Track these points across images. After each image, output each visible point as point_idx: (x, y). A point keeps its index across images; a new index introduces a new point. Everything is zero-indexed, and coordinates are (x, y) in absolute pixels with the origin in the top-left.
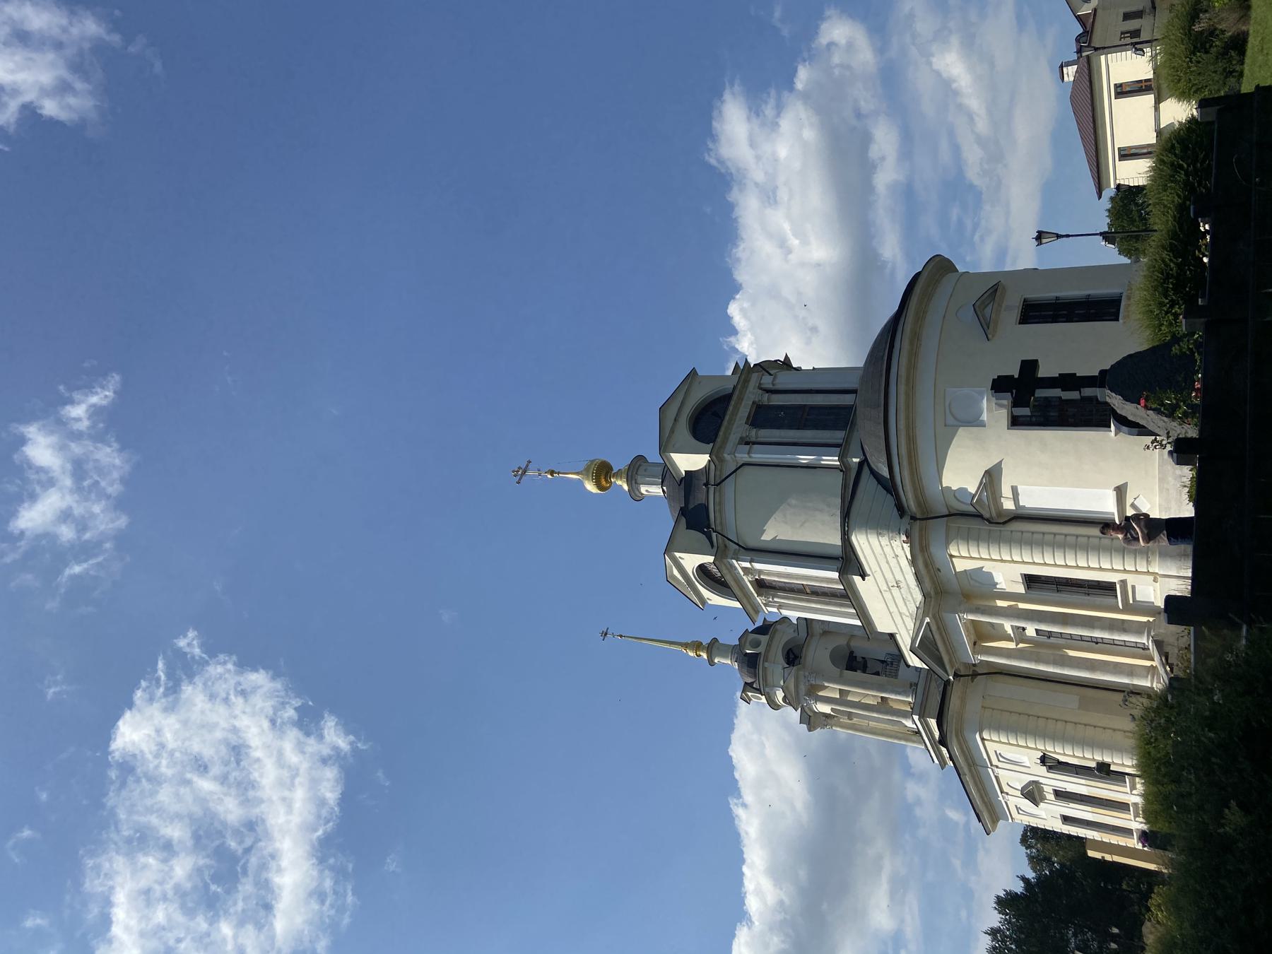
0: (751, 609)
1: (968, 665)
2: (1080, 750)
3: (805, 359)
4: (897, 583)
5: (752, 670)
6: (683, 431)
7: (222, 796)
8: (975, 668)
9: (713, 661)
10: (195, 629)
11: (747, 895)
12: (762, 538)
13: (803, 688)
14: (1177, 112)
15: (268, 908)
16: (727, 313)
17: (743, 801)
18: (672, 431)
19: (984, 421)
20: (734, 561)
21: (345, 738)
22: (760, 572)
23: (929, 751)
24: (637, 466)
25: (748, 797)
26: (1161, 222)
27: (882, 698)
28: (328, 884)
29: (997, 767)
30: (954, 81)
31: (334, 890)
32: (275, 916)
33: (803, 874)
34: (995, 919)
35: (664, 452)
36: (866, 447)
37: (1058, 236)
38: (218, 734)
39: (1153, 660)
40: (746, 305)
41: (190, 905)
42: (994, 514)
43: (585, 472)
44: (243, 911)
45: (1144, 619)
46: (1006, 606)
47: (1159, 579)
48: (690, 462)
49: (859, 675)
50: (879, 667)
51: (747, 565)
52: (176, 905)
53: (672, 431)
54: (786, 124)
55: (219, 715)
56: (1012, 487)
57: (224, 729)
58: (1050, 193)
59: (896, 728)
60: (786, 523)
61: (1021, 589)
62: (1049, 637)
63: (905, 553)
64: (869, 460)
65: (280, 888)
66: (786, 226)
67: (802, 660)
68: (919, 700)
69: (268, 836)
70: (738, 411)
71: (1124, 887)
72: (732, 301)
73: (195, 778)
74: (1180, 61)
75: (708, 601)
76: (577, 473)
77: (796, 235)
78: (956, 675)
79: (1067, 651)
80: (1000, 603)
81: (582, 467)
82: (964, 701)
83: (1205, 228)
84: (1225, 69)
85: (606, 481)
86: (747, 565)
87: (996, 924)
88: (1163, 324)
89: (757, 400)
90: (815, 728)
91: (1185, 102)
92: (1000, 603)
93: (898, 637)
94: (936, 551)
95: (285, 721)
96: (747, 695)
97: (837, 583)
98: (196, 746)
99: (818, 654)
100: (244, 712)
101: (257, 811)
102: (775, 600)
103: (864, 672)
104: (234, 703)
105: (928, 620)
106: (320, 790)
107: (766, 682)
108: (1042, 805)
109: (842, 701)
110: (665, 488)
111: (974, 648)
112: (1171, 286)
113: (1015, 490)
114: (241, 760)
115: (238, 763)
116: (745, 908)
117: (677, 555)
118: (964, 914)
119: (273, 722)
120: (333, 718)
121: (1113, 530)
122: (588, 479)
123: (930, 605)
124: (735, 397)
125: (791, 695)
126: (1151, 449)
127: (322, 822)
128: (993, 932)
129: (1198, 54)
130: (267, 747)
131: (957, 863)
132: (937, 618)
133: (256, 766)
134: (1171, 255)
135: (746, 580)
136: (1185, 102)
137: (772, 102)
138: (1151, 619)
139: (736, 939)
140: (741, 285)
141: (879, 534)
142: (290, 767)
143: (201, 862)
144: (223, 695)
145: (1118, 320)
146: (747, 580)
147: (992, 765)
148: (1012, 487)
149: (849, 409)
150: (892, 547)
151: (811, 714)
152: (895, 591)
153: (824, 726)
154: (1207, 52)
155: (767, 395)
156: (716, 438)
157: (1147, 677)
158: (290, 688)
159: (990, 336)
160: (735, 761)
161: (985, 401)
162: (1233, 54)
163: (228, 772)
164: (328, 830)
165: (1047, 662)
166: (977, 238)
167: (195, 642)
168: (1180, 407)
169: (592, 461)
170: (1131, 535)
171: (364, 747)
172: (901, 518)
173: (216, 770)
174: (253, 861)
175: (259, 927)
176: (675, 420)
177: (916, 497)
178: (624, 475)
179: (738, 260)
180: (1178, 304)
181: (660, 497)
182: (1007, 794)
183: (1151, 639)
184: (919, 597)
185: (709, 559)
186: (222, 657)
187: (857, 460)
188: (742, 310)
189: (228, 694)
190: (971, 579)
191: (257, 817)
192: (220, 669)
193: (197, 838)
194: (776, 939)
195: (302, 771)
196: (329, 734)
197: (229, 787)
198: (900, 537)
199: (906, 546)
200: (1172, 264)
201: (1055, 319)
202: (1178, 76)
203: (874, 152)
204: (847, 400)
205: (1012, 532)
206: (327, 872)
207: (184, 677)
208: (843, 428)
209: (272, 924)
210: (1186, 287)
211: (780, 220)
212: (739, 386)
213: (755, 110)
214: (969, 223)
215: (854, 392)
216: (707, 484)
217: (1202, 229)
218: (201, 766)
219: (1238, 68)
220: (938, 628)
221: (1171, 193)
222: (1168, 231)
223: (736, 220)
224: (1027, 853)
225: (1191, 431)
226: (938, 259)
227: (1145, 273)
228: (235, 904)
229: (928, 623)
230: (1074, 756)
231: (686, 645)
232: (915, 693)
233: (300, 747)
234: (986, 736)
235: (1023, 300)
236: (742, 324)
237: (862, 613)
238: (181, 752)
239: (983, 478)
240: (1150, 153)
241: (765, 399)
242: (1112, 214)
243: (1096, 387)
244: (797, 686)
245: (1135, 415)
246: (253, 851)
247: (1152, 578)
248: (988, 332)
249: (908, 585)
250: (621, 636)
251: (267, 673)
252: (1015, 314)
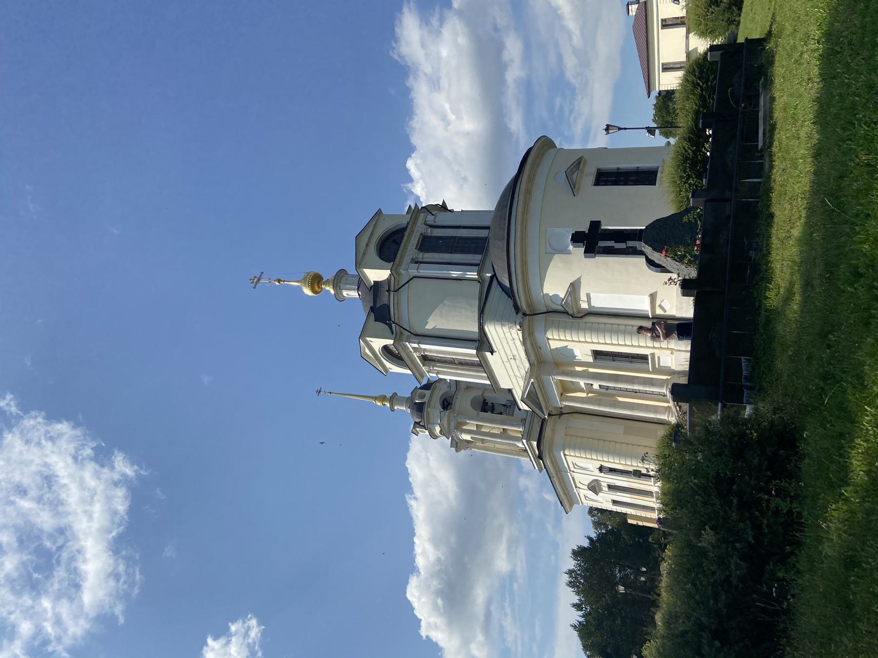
0: (418, 374)
1: (556, 408)
2: (624, 459)
3: (456, 205)
4: (513, 356)
5: (420, 413)
6: (372, 251)
7: (39, 511)
8: (561, 410)
9: (393, 409)
10: (11, 393)
11: (417, 556)
12: (426, 328)
13: (453, 424)
14: (700, 45)
15: (77, 587)
16: (406, 167)
17: (414, 496)
18: (364, 254)
19: (570, 250)
20: (407, 343)
21: (131, 468)
22: (425, 350)
23: (532, 462)
24: (340, 277)
25: (418, 493)
26: (684, 121)
27: (503, 429)
28: (121, 568)
29: (573, 472)
30: (560, 9)
31: (126, 572)
32: (83, 592)
33: (453, 539)
34: (571, 564)
35: (359, 268)
36: (495, 266)
37: (620, 129)
38: (34, 468)
39: (669, 403)
40: (419, 161)
41: (18, 587)
42: (575, 311)
43: (303, 281)
44: (59, 590)
45: (665, 377)
46: (581, 370)
47: (675, 352)
48: (377, 275)
49: (489, 415)
50: (502, 409)
51: (416, 345)
52: (7, 589)
53: (364, 254)
54: (446, 32)
55: (33, 455)
56: (587, 294)
57: (38, 464)
58: (619, 90)
59: (512, 448)
60: (442, 317)
61: (590, 359)
62: (607, 389)
63: (519, 337)
64: (497, 276)
65: (85, 572)
66: (447, 106)
67: (453, 406)
68: (527, 430)
69: (75, 537)
70: (410, 240)
71: (650, 539)
72: (409, 158)
73: (18, 500)
74: (701, 11)
75: (390, 370)
76: (298, 282)
77: (453, 112)
78: (549, 415)
79: (618, 398)
80: (578, 369)
81: (302, 276)
82: (555, 431)
83: (709, 133)
84: (729, 19)
85: (319, 287)
86: (416, 345)
87: (572, 567)
88: (682, 191)
89: (423, 232)
90: (460, 450)
91: (703, 39)
92: (578, 369)
93: (514, 391)
94: (538, 335)
95: (85, 457)
96: (416, 430)
97: (475, 357)
98: (17, 477)
99: (463, 402)
100: (53, 452)
101: (65, 520)
102: (435, 368)
103: (492, 413)
104: (45, 446)
105: (532, 380)
106: (113, 504)
108: (600, 494)
109: (478, 432)
110: (360, 293)
111: (561, 397)
112: (688, 165)
113: (588, 296)
114: (52, 486)
115: (50, 487)
116: (415, 564)
117: (368, 339)
118: (553, 557)
119: (75, 458)
120: (121, 454)
121: (645, 330)
122: (305, 286)
123: (534, 371)
124: (408, 230)
125: (446, 431)
126: (668, 284)
127: (115, 526)
128: (570, 572)
129: (713, 7)
130: (71, 476)
131: (549, 527)
132: (539, 380)
133: (64, 490)
134: (689, 144)
135: (415, 356)
136: (703, 39)
137: (437, 16)
138: (669, 377)
139: (409, 585)
140: (415, 147)
141: (502, 325)
142: (89, 489)
143: (25, 558)
144: (36, 440)
145: (655, 185)
146: (416, 355)
147: (570, 471)
148: (587, 294)
149: (485, 240)
150: (511, 333)
151: (458, 441)
152: (512, 361)
153: (466, 448)
154: (718, 6)
155: (430, 229)
156: (395, 258)
157: (665, 413)
158: (87, 434)
159: (575, 193)
160: (409, 470)
162: (734, 9)
163: (42, 495)
164: (121, 531)
165: (605, 406)
166: (571, 119)
167: (12, 403)
168: (686, 257)
169: (308, 273)
170: (656, 334)
171: (146, 474)
172: (517, 314)
173: (33, 493)
174: (65, 555)
175: (71, 600)
176: (367, 245)
177: (527, 301)
178: (331, 283)
179: (413, 129)
180: (692, 177)
181: (356, 298)
182: (579, 488)
183: (668, 390)
184: (527, 365)
185: (390, 342)
186: (33, 413)
187: (490, 275)
188: (416, 165)
189: (40, 440)
190: (561, 353)
191: (66, 525)
192: (32, 422)
193: (21, 541)
194: (435, 583)
195: (99, 491)
196: (118, 465)
197: (44, 504)
198: (516, 327)
199: (520, 333)
200: (689, 151)
201: (616, 183)
202: (699, 20)
203: (506, 56)
204: (483, 233)
205: (586, 323)
206: (120, 560)
207: (5, 428)
208: (481, 253)
209: (81, 598)
210: (698, 166)
211: (443, 102)
212: (411, 223)
213: (425, 21)
214: (567, 109)
215: (487, 228)
216: (388, 291)
217: (707, 133)
218: (22, 491)
219: (737, 19)
220: (539, 386)
221: (691, 102)
222: (688, 128)
223: (412, 100)
224: (592, 520)
225: (692, 273)
226: (544, 139)
227: (672, 156)
228: (52, 585)
229: (532, 382)
230: (620, 464)
231: (375, 398)
232: (524, 425)
233: (97, 475)
234: (567, 452)
235: (597, 170)
236: (416, 174)
237: (491, 376)
238: (5, 482)
239: (568, 288)
240: (681, 68)
241: (430, 232)
242: (657, 108)
243: (636, 240)
244: (449, 423)
245: (659, 260)
246: (64, 549)
247: (670, 352)
248: (574, 191)
249: (520, 357)
250: (330, 393)
251: (70, 424)
252: (592, 179)
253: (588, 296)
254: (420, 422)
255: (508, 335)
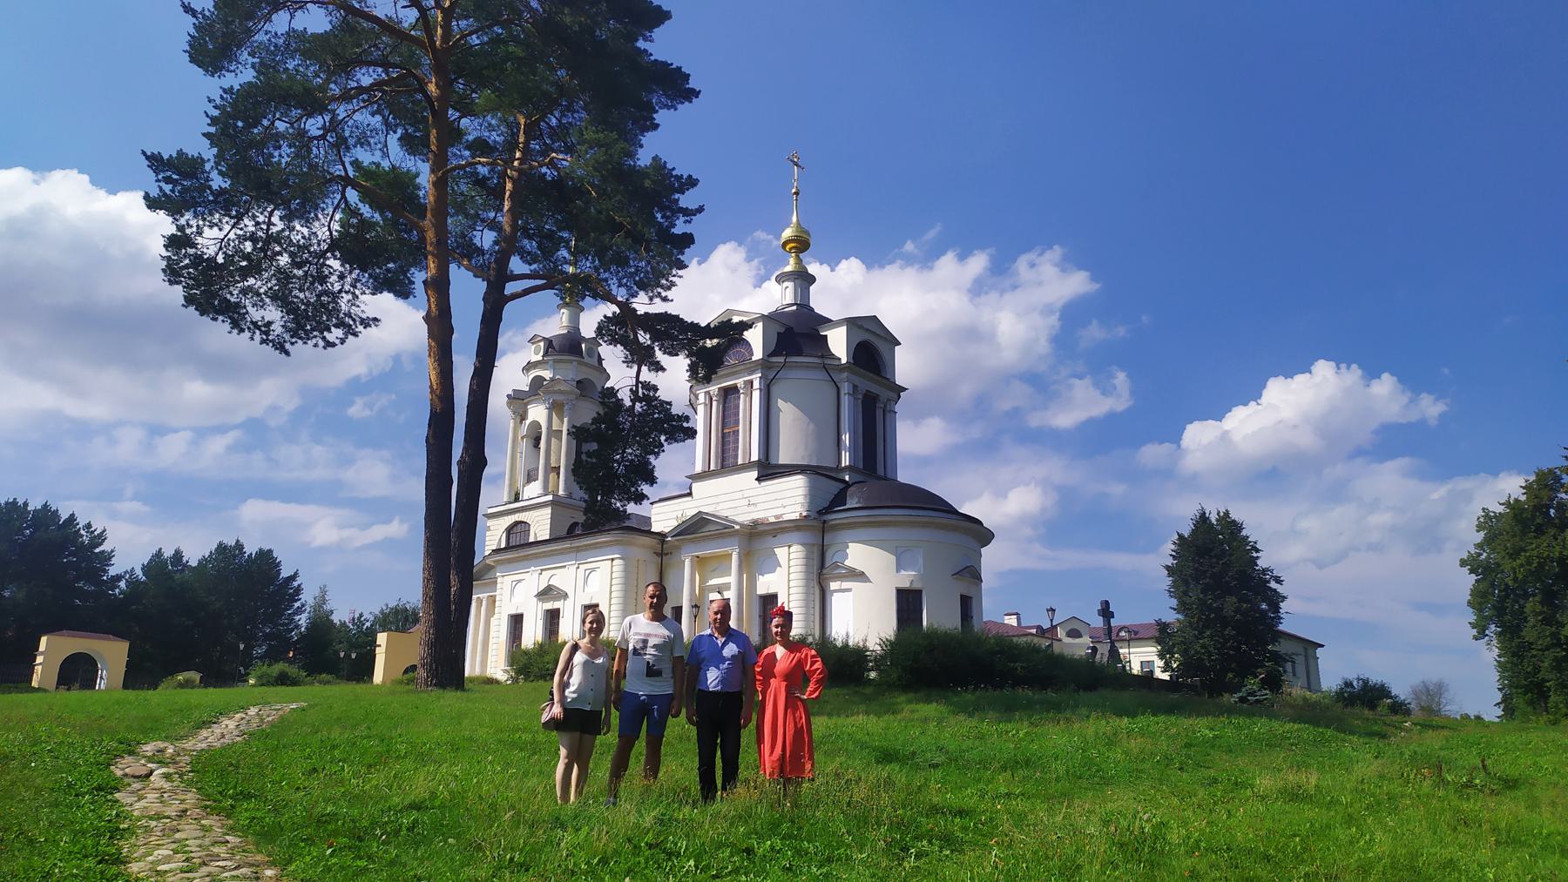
12: (779, 400)
13: (560, 398)
20: (760, 375)
76: (798, 220)
85: (791, 249)
86: (756, 384)
94: (796, 535)
96: (539, 341)
107: (557, 362)
124: (877, 378)
146: (740, 382)
161: (914, 573)
169: (809, 235)
244: (560, 392)
253: (849, 590)
254: (554, 348)
255: (792, 501)
